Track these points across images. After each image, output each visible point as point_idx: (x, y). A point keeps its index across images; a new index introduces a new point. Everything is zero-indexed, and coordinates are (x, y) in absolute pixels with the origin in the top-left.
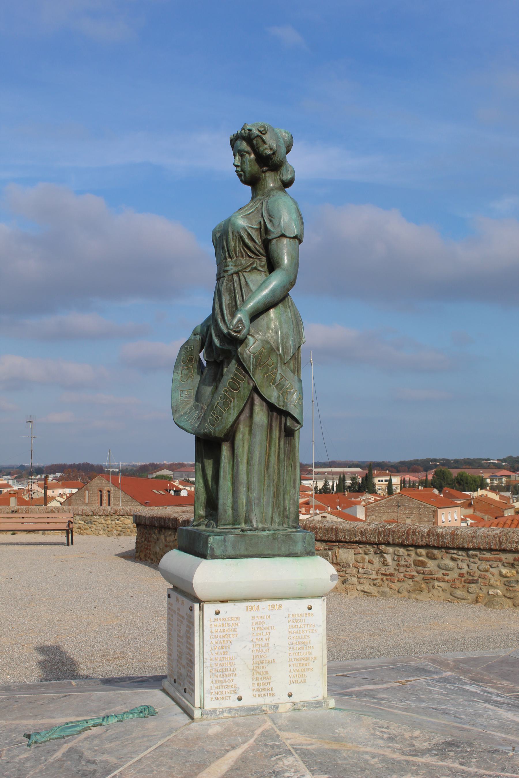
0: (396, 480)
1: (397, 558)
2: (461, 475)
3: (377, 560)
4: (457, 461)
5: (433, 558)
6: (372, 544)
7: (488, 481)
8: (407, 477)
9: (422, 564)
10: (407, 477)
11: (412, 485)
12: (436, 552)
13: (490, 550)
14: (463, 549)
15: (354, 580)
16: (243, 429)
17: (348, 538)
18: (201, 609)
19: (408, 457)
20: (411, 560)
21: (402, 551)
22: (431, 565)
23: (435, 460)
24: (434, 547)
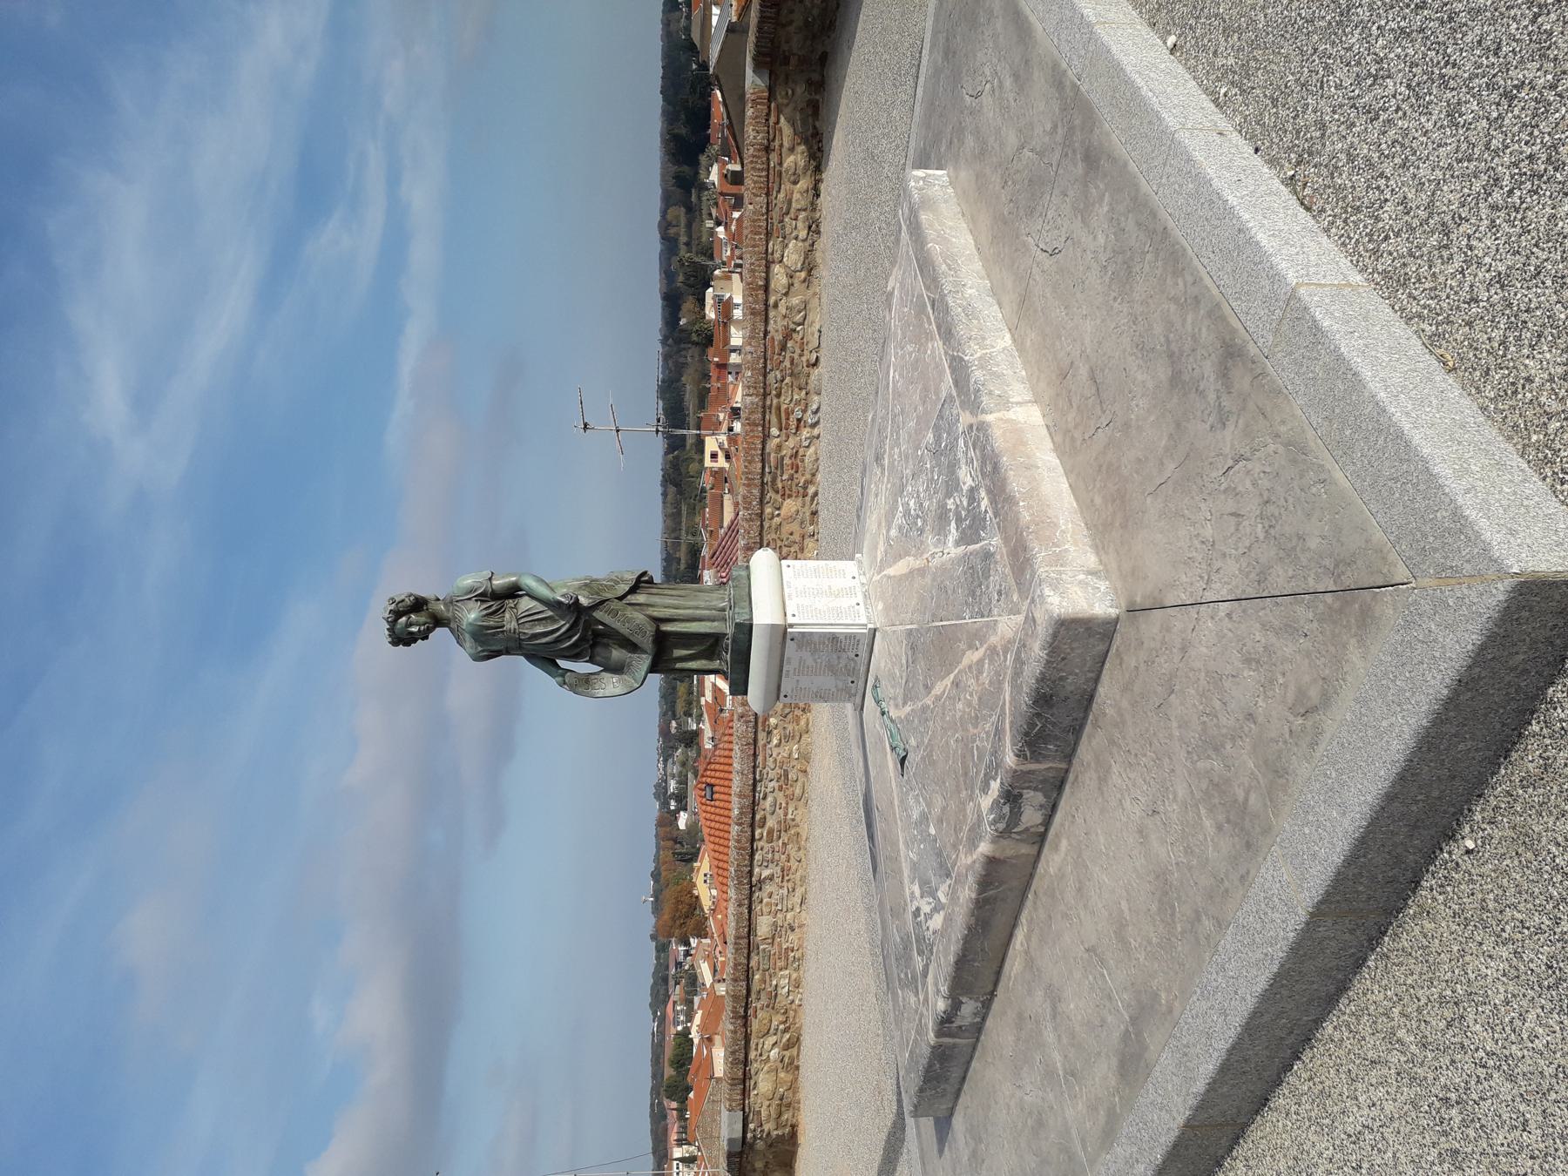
0: (678, 1153)
1: (766, 863)
2: (672, 1063)
3: (768, 888)
4: (654, 1076)
5: (764, 820)
6: (751, 893)
7: (680, 1028)
8: (674, 1137)
9: (770, 832)
10: (674, 1137)
11: (684, 1129)
12: (758, 817)
13: (755, 755)
14: (754, 785)
15: (789, 915)
16: (650, 611)
17: (746, 923)
18: (791, 626)
19: (648, 1144)
20: (767, 846)
21: (757, 857)
22: (771, 823)
23: (652, 1105)
24: (753, 818)
